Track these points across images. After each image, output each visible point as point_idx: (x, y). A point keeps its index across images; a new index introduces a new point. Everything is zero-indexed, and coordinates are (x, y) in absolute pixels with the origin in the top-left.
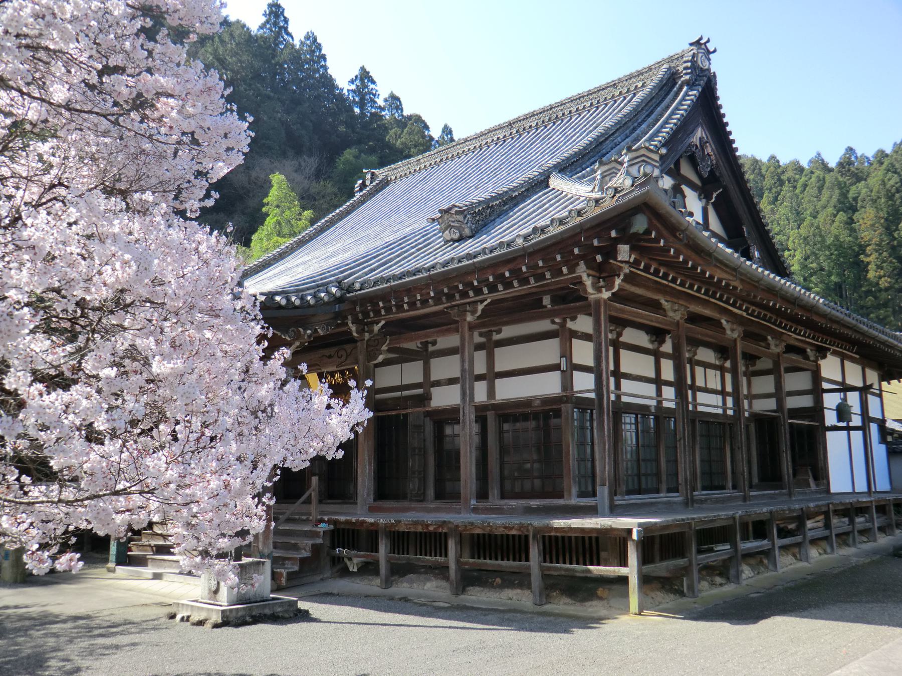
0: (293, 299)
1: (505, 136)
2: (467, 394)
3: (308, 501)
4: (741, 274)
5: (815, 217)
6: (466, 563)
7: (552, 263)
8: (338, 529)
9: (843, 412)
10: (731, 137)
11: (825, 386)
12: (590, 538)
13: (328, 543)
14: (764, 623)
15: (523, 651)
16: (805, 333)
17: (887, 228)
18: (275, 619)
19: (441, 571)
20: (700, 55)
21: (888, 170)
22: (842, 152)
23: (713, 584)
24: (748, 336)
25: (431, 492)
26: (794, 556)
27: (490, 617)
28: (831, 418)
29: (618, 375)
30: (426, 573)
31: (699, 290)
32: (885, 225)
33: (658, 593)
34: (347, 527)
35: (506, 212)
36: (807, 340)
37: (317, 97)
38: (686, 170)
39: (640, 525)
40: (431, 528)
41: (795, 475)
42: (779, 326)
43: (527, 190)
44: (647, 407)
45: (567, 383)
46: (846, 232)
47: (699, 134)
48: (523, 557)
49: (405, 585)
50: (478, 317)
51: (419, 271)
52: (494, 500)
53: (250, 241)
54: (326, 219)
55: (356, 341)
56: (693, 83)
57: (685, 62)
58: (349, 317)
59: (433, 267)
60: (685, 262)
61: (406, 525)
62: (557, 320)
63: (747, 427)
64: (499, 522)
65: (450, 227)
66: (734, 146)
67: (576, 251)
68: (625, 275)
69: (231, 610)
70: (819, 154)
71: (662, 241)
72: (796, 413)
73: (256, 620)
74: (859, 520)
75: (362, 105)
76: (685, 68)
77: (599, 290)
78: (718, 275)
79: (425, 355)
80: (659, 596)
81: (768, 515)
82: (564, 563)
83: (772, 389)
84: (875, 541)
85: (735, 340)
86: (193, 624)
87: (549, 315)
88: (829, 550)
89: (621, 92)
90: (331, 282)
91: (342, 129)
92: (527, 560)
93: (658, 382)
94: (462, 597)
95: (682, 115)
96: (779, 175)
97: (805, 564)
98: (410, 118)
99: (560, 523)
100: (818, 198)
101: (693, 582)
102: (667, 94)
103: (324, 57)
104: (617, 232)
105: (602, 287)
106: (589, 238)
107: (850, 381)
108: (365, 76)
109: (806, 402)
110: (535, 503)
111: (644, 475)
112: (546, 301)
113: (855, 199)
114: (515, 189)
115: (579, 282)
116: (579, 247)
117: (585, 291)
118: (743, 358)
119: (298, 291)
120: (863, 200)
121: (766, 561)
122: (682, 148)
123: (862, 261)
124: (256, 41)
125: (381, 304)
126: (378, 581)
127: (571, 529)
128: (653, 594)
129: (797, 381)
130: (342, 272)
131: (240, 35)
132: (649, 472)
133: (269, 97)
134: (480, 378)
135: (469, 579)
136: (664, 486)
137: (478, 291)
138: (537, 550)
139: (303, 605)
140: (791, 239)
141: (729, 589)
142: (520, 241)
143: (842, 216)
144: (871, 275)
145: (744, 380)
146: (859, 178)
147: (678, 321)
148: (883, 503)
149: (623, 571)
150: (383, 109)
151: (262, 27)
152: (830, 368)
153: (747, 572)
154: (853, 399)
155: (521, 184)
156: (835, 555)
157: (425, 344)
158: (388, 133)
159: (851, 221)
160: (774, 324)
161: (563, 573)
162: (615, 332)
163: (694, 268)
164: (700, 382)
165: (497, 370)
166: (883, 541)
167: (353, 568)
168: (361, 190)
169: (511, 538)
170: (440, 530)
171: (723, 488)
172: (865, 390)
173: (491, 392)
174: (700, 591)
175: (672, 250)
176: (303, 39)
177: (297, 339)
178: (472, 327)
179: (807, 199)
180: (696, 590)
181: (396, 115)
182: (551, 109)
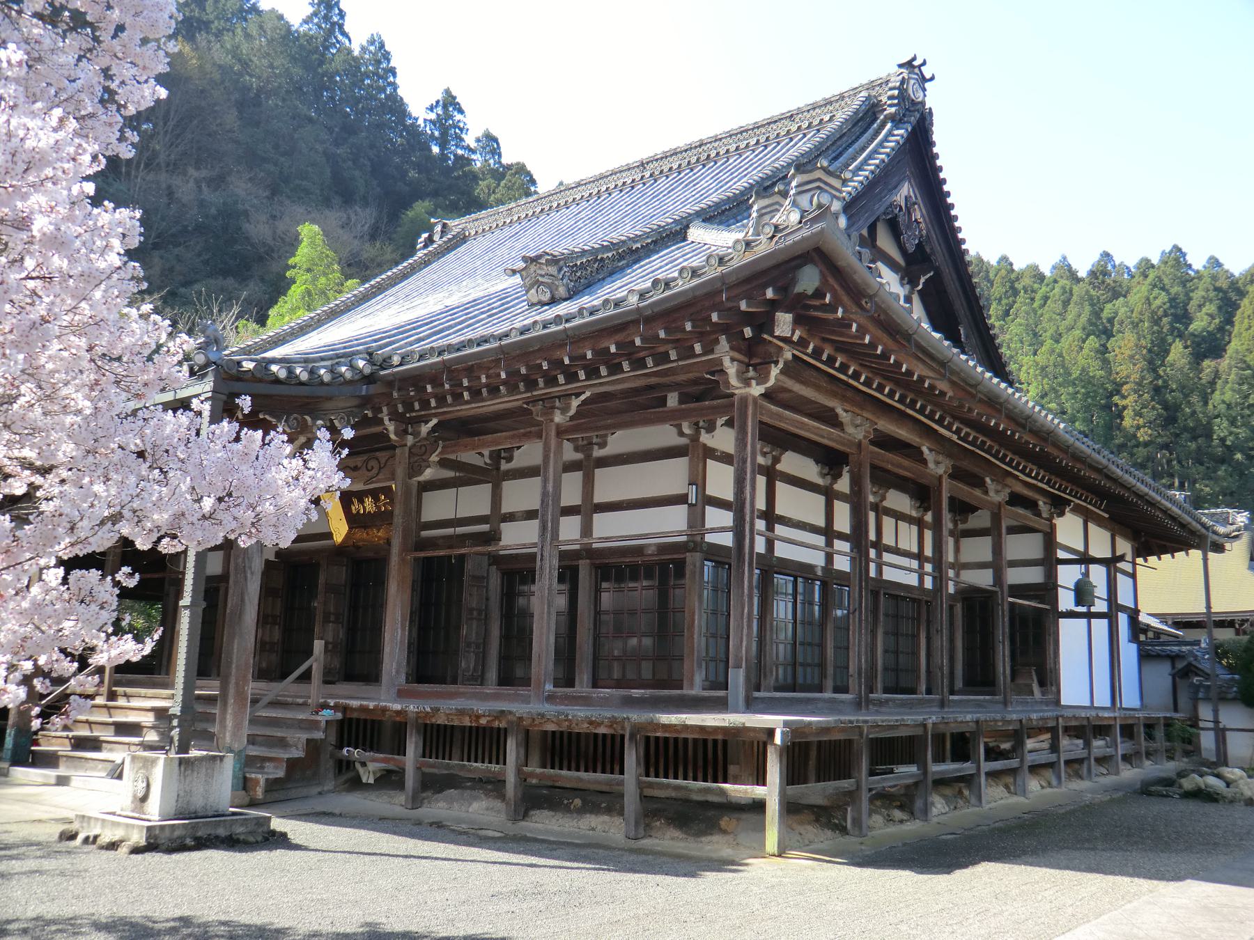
0: (298, 371)
1: (633, 181)
2: (549, 531)
3: (306, 677)
4: (953, 372)
5: (1057, 341)
6: (532, 775)
7: (679, 336)
8: (351, 719)
9: (1082, 592)
10: (949, 200)
11: (1061, 554)
12: (715, 741)
13: (333, 739)
14: (959, 874)
15: (598, 899)
16: (1038, 474)
17: (1151, 362)
18: (232, 843)
19: (494, 786)
20: (912, 82)
21: (1155, 286)
22: (1097, 257)
23: (890, 820)
24: (957, 475)
25: (492, 674)
26: (1007, 787)
27: (559, 852)
28: (1066, 601)
29: (770, 517)
31: (891, 395)
32: (1148, 356)
33: (810, 828)
35: (622, 269)
36: (1040, 484)
37: (380, 126)
38: (884, 241)
39: (786, 724)
40: (483, 721)
41: (1013, 679)
42: (1002, 460)
43: (655, 242)
44: (810, 568)
45: (696, 520)
46: (1097, 364)
47: (906, 191)
48: (617, 768)
49: (441, 804)
50: (572, 418)
51: (486, 341)
52: (582, 687)
53: (267, 317)
54: (372, 283)
55: (394, 448)
56: (900, 120)
57: (891, 89)
58: (385, 409)
59: (507, 335)
60: (873, 345)
61: (447, 715)
63: (951, 608)
64: (582, 714)
65: (537, 283)
66: (953, 213)
67: (715, 317)
68: (786, 363)
69: (162, 827)
70: (1065, 258)
71: (840, 310)
72: (1020, 590)
73: (201, 844)
74: (1098, 744)
75: (443, 144)
76: (890, 98)
77: (747, 382)
78: (919, 371)
79: (493, 475)
80: (811, 831)
81: (973, 725)
82: (676, 777)
83: (988, 557)
84: (1117, 773)
85: (941, 477)
86: (102, 848)
87: (674, 417)
88: (1054, 782)
89: (799, 127)
90: (358, 352)
91: (413, 174)
92: (622, 772)
93: (829, 532)
94: (523, 823)
95: (883, 161)
96: (1012, 282)
97: (1021, 799)
98: (509, 167)
100: (1062, 315)
101: (860, 813)
102: (863, 133)
103: (393, 71)
104: (775, 291)
107: (1095, 552)
108: (450, 102)
109: (1033, 576)
110: (636, 693)
111: (802, 665)
112: (673, 400)
113: (1111, 320)
114: (636, 239)
116: (719, 311)
117: (727, 383)
118: (950, 511)
119: (306, 361)
120: (1121, 323)
121: (966, 792)
122: (880, 208)
123: (1116, 405)
124: (297, 39)
125: (429, 389)
126: (401, 798)
127: (686, 727)
128: (801, 829)
129: (1023, 547)
130: (375, 341)
131: (274, 29)
132: (809, 661)
133: (310, 120)
134: (569, 511)
135: (534, 799)
136: (829, 683)
137: (572, 377)
139: (277, 824)
140: (1024, 369)
141: (913, 827)
142: (634, 299)
143: (1093, 342)
144: (1128, 422)
145: (951, 541)
146: (1116, 293)
147: (860, 442)
148: (1130, 722)
149: (758, 791)
150: (473, 151)
151: (306, 22)
152: (1069, 530)
153: (939, 806)
154: (1098, 575)
155: (645, 233)
156: (1063, 789)
157: (496, 457)
158: (477, 184)
159: (1104, 350)
161: (673, 794)
162: (769, 456)
163: (885, 356)
164: (888, 540)
165: (597, 500)
166: (1129, 774)
167: (367, 778)
168: (426, 246)
169: (600, 738)
170: (496, 724)
171: (913, 691)
172: (1111, 563)
173: (587, 530)
174: (870, 828)
175: (854, 326)
176: (365, 43)
177: (301, 433)
178: (561, 432)
179: (1046, 316)
180: (864, 826)
181: (492, 161)
182: (700, 146)
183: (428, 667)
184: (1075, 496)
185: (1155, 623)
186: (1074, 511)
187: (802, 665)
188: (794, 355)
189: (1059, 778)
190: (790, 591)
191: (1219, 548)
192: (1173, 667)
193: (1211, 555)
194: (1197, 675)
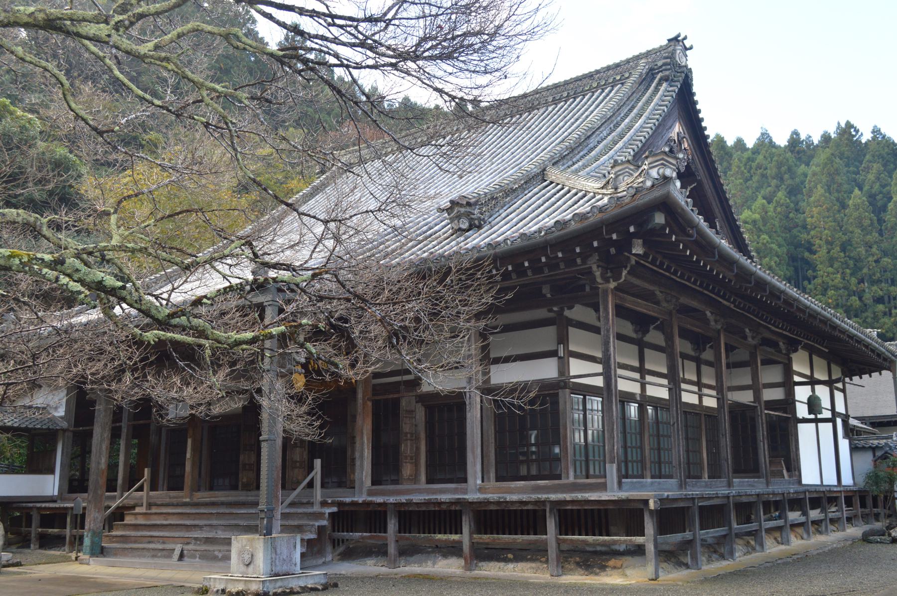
9: (813, 404)
11: (797, 379)
16: (783, 325)
19: (454, 550)
20: (678, 52)
26: (775, 539)
28: (802, 411)
30: (433, 552)
34: (352, 509)
40: (444, 507)
43: (526, 183)
47: (677, 128)
62: (555, 309)
68: (632, 267)
72: (771, 405)
77: (607, 281)
83: (750, 382)
88: (805, 536)
99: (384, 570)
105: (609, 277)
106: (610, 232)
107: (818, 376)
109: (776, 394)
112: (546, 291)
115: (589, 272)
136: (648, 473)
160: (757, 316)
184: (807, 339)
186: (803, 348)
187: (632, 462)
190: (581, 408)
192: (874, 456)
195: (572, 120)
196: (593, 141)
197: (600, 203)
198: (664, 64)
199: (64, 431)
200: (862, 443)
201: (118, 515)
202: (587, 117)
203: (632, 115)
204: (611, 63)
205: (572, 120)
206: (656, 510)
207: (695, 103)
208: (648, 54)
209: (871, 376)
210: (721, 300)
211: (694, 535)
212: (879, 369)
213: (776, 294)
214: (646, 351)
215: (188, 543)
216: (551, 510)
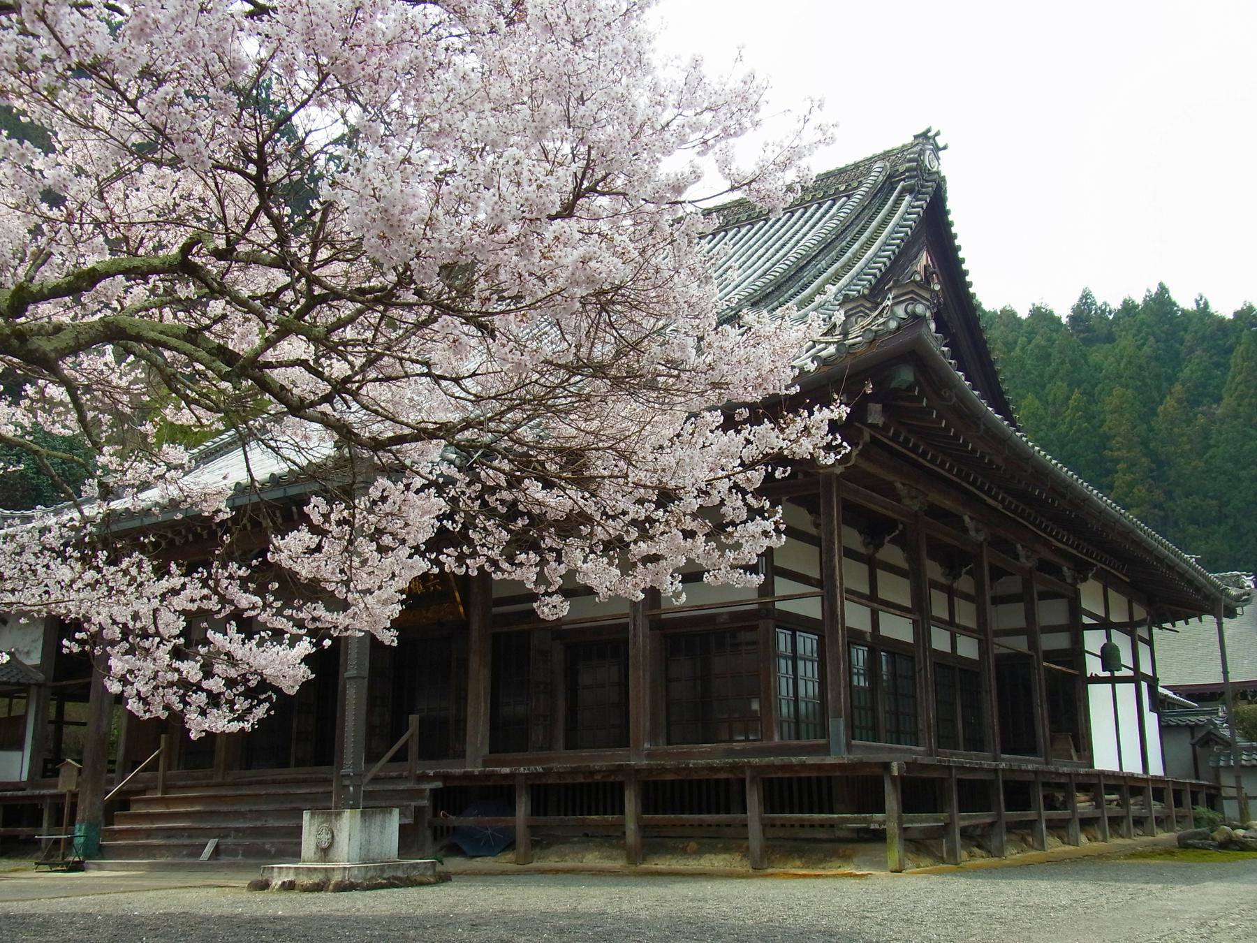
11: (1086, 620)
16: (1068, 539)
20: (928, 152)
28: (1094, 666)
31: (950, 470)
36: (1070, 550)
40: (598, 777)
47: (924, 259)
60: (947, 428)
68: (865, 444)
72: (1051, 655)
83: (1022, 623)
88: (1100, 837)
107: (1114, 618)
109: (1058, 642)
129: (1052, 612)
138: (756, 798)
152: (1091, 598)
163: (956, 437)
183: (506, 736)
184: (1100, 561)
185: (1166, 692)
186: (1095, 577)
188: (872, 437)
189: (1104, 834)
191: (1231, 613)
192: (1193, 738)
193: (1225, 620)
194: (1217, 743)
195: (777, 246)
196: (807, 274)
197: (824, 354)
198: (908, 170)
199: (39, 685)
200: (1173, 721)
201: (122, 802)
202: (798, 242)
203: (863, 238)
204: (832, 168)
205: (777, 246)
206: (902, 778)
207: (950, 224)
208: (885, 156)
209: (1187, 623)
210: (985, 497)
211: (951, 817)
212: (1198, 612)
213: (1062, 489)
214: (880, 574)
215: (226, 836)
216: (752, 781)
